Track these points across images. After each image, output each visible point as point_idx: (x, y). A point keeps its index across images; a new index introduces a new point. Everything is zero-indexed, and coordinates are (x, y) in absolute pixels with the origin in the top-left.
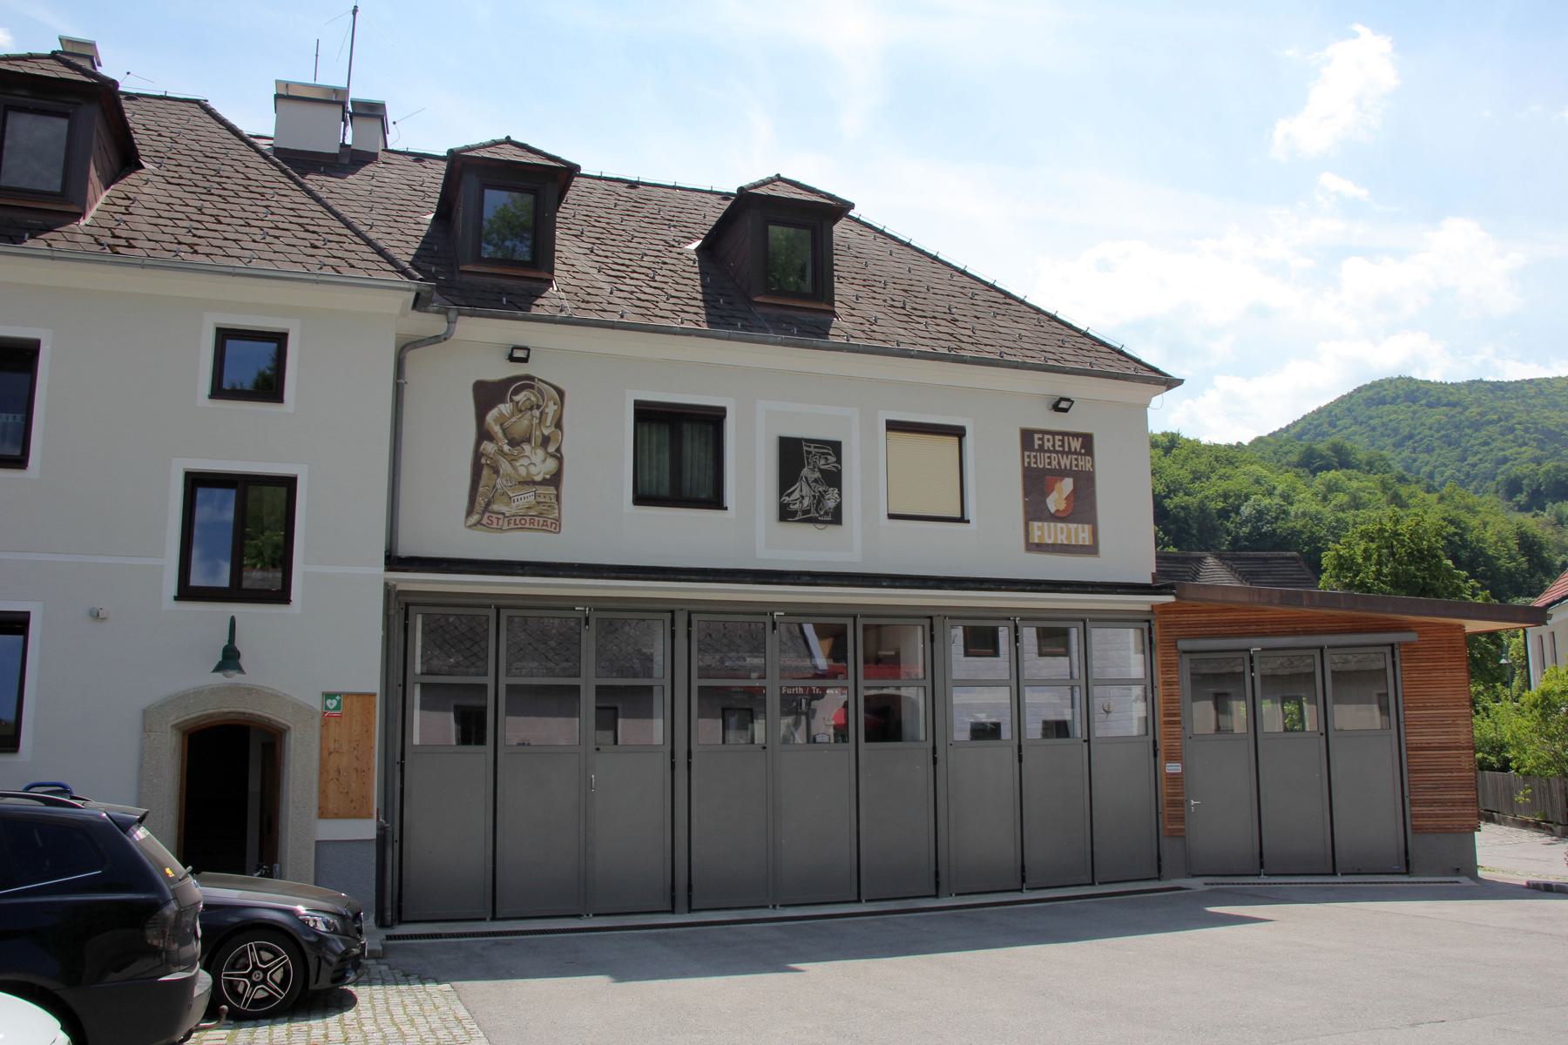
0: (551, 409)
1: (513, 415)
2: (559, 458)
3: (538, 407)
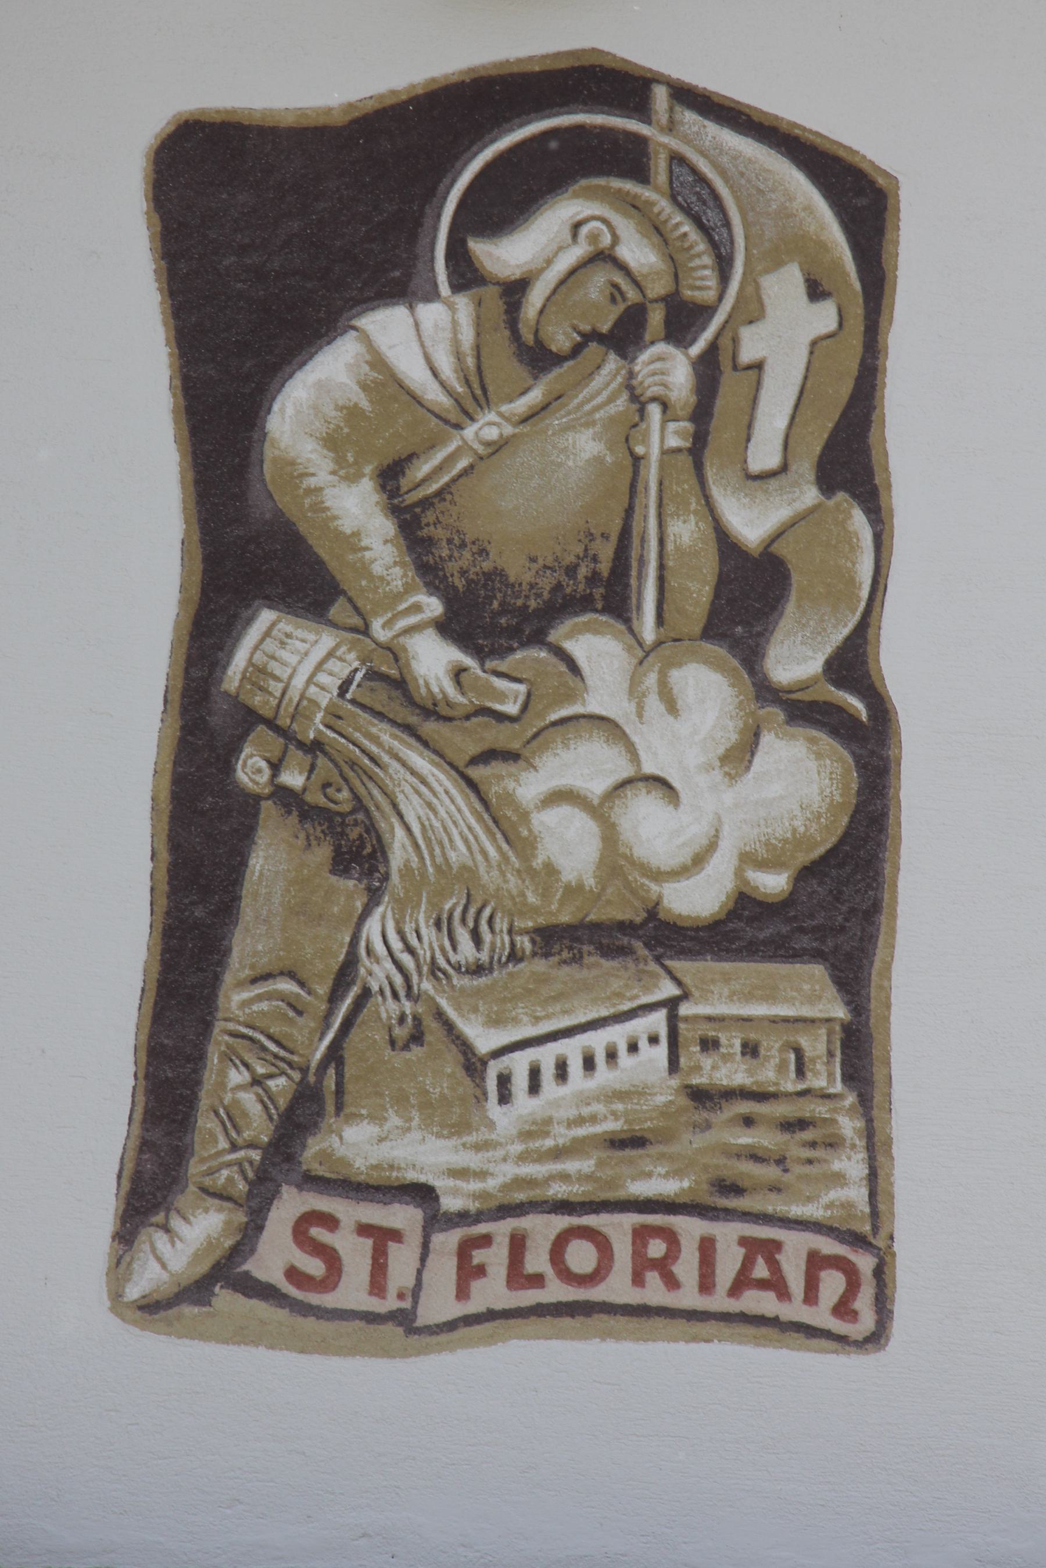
0: (786, 333)
1: (477, 393)
2: (852, 713)
3: (683, 319)
